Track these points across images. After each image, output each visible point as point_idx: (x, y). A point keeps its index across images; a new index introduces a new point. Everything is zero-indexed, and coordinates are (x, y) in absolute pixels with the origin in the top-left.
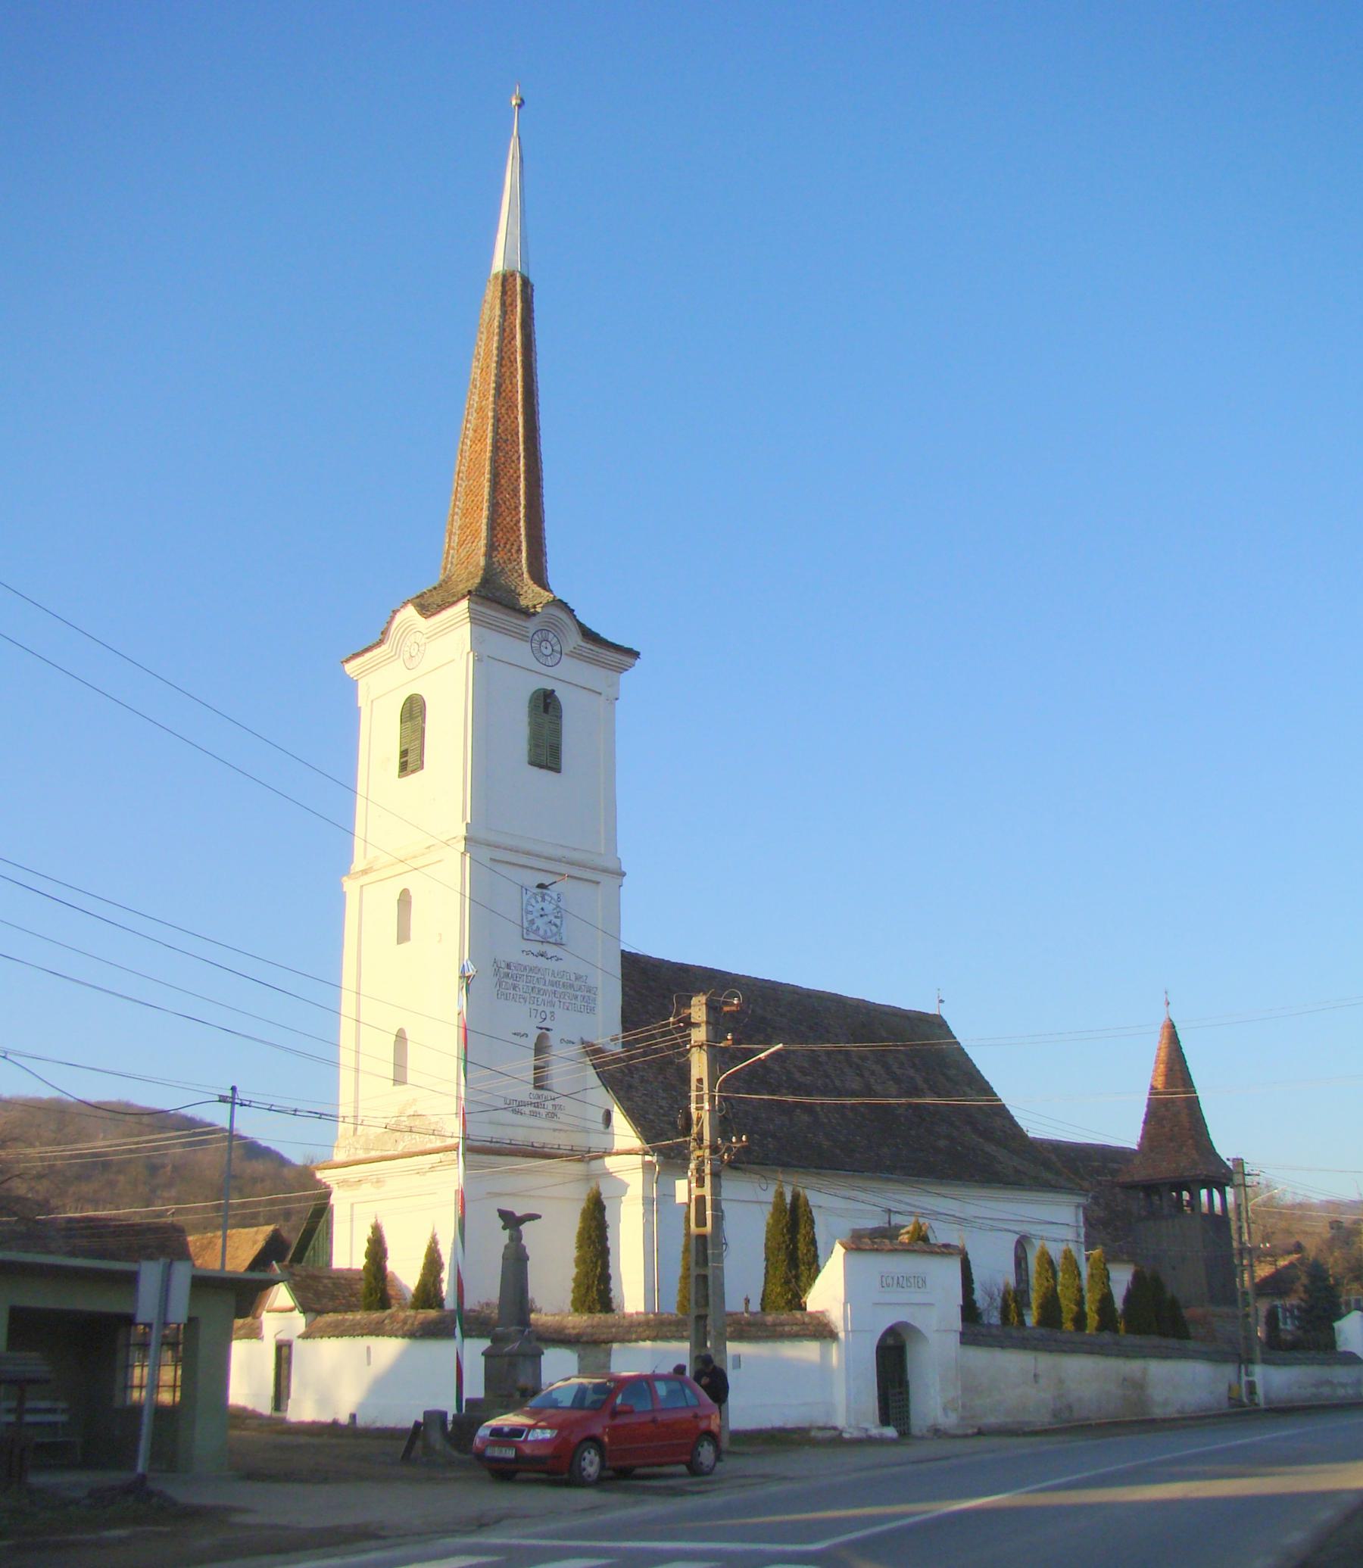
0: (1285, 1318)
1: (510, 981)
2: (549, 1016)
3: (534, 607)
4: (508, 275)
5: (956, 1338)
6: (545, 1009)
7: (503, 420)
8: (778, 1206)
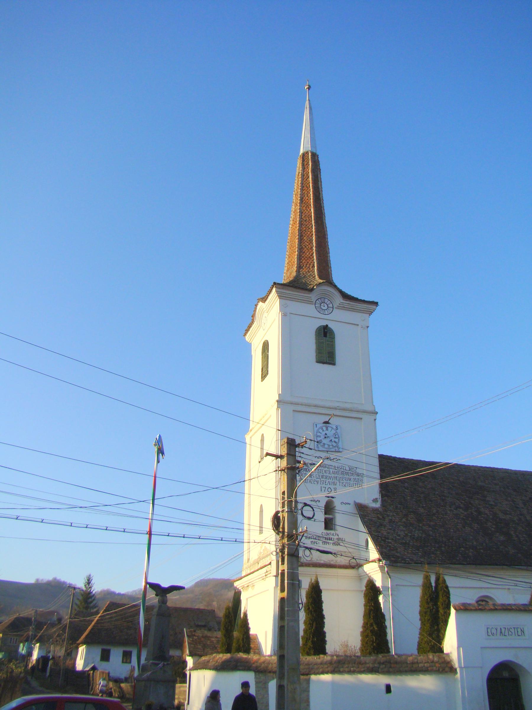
4: (305, 153)
6: (330, 486)
8: (426, 585)
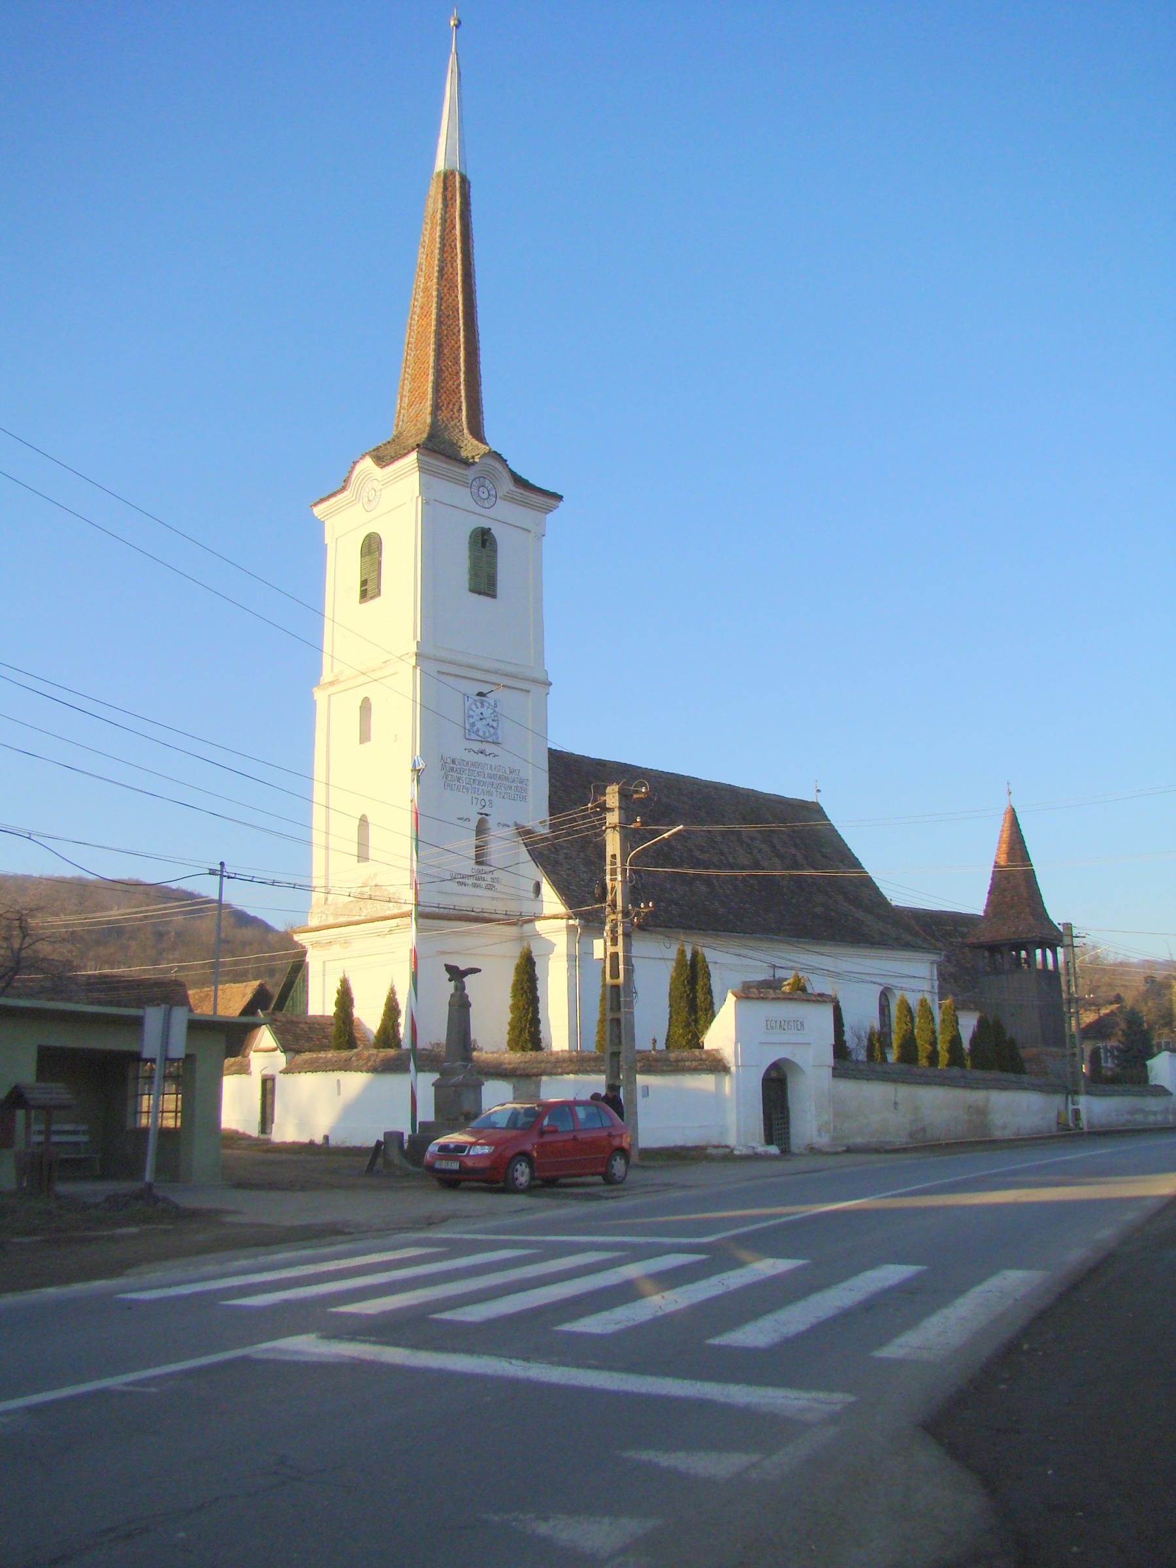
0: (1106, 1058)
1: (455, 775)
2: (487, 804)
3: (473, 457)
5: (829, 1072)
7: (445, 298)
8: (681, 962)
